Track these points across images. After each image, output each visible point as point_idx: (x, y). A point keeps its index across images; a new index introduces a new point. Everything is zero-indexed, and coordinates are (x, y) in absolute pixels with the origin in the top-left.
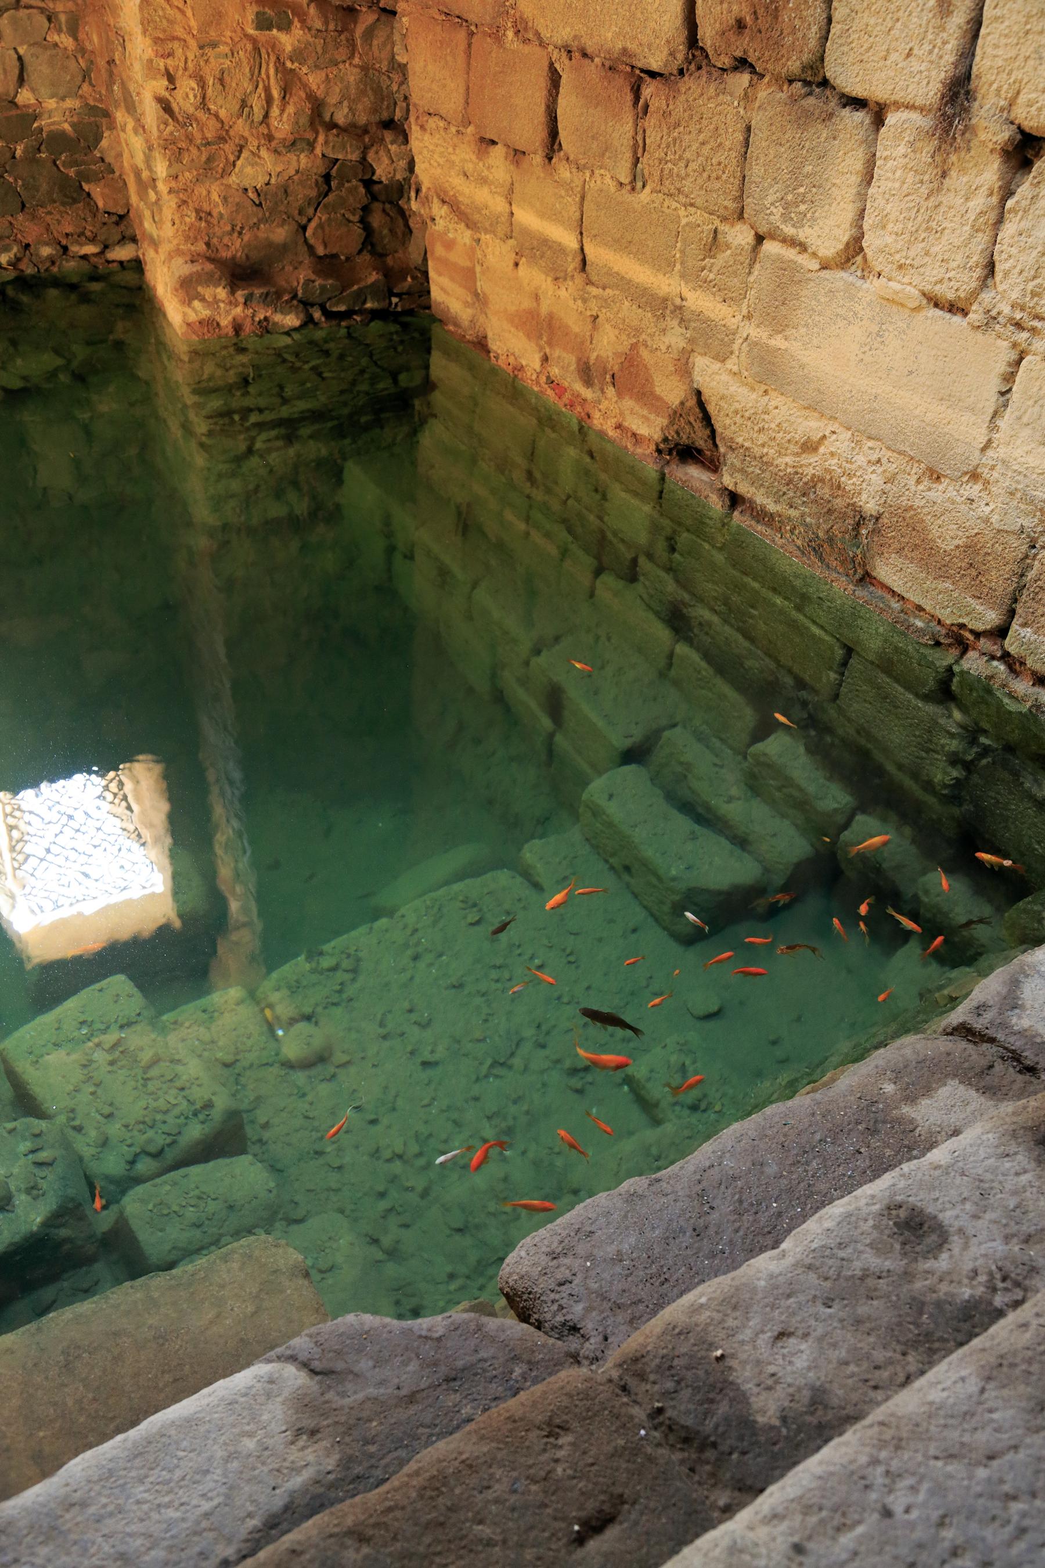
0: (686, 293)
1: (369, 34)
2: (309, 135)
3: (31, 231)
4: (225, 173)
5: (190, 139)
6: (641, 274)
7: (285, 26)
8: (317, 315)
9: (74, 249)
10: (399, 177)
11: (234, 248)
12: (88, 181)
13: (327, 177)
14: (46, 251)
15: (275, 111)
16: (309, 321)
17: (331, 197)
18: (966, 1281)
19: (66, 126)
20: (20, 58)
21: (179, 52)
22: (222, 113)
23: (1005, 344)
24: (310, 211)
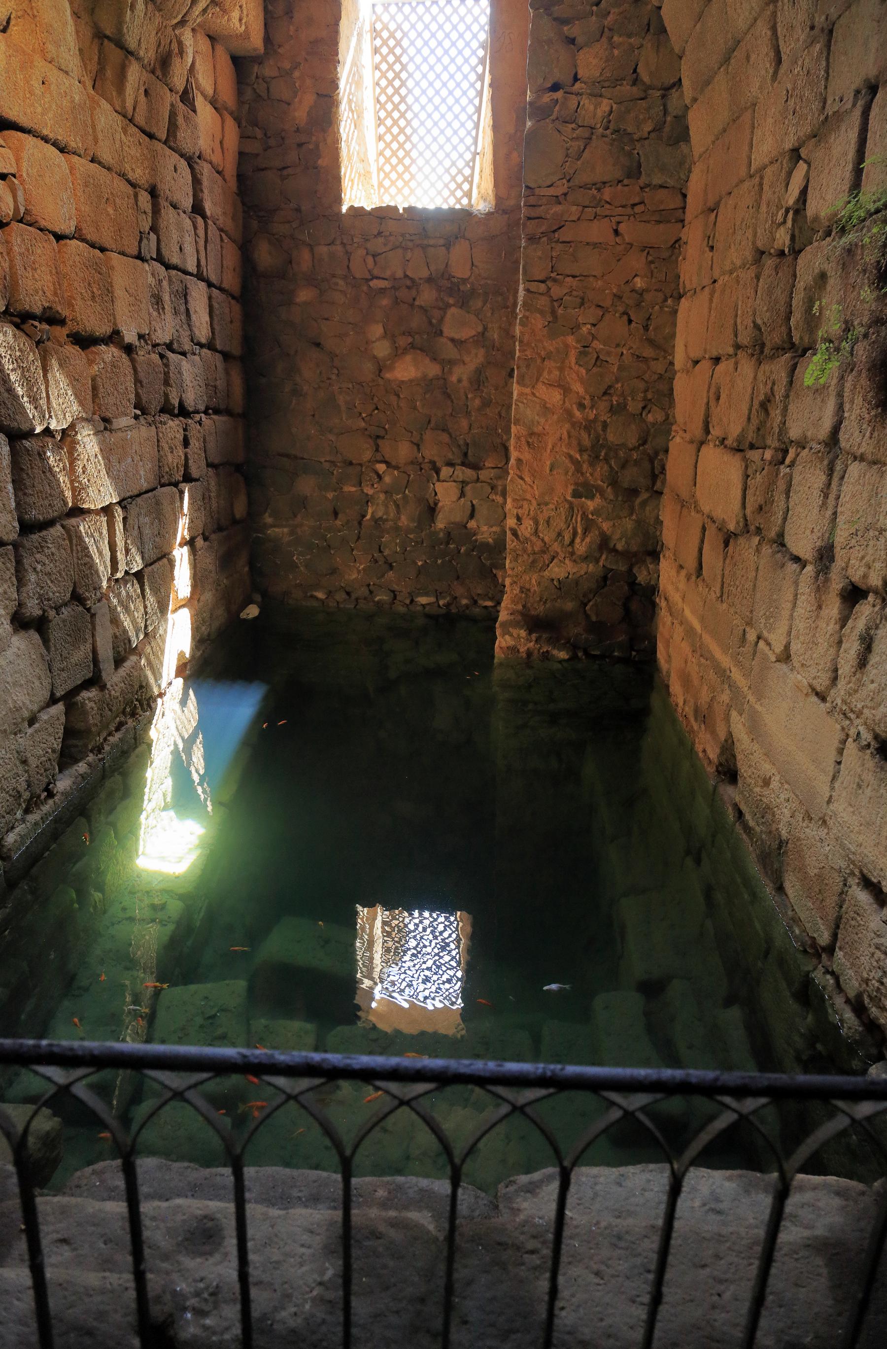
0: (733, 669)
1: (644, 503)
2: (597, 555)
3: (459, 590)
4: (542, 569)
5: (525, 550)
6: (718, 653)
7: (592, 497)
8: (580, 654)
9: (480, 602)
10: (652, 583)
11: (540, 610)
12: (496, 568)
13: (605, 578)
14: (464, 602)
15: (578, 540)
16: (574, 658)
17: (606, 589)
18: (190, 1280)
19: (490, 540)
20: (473, 506)
21: (526, 506)
22: (546, 539)
23: (838, 727)
24: (591, 596)
